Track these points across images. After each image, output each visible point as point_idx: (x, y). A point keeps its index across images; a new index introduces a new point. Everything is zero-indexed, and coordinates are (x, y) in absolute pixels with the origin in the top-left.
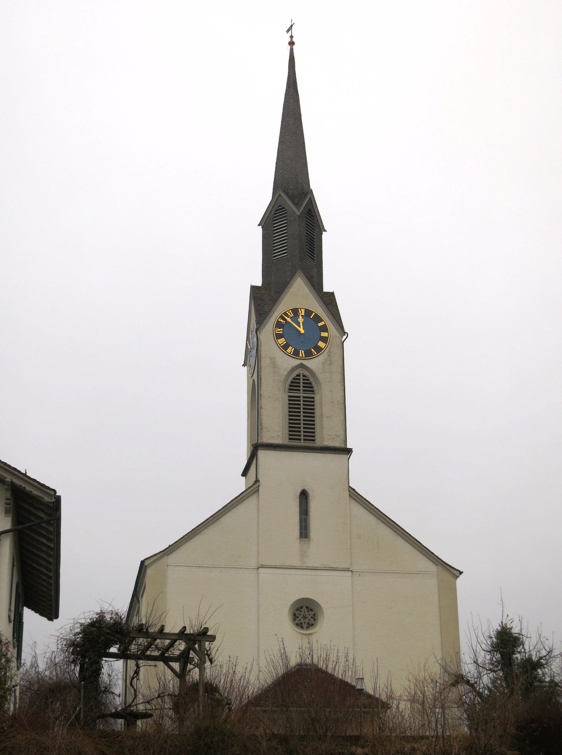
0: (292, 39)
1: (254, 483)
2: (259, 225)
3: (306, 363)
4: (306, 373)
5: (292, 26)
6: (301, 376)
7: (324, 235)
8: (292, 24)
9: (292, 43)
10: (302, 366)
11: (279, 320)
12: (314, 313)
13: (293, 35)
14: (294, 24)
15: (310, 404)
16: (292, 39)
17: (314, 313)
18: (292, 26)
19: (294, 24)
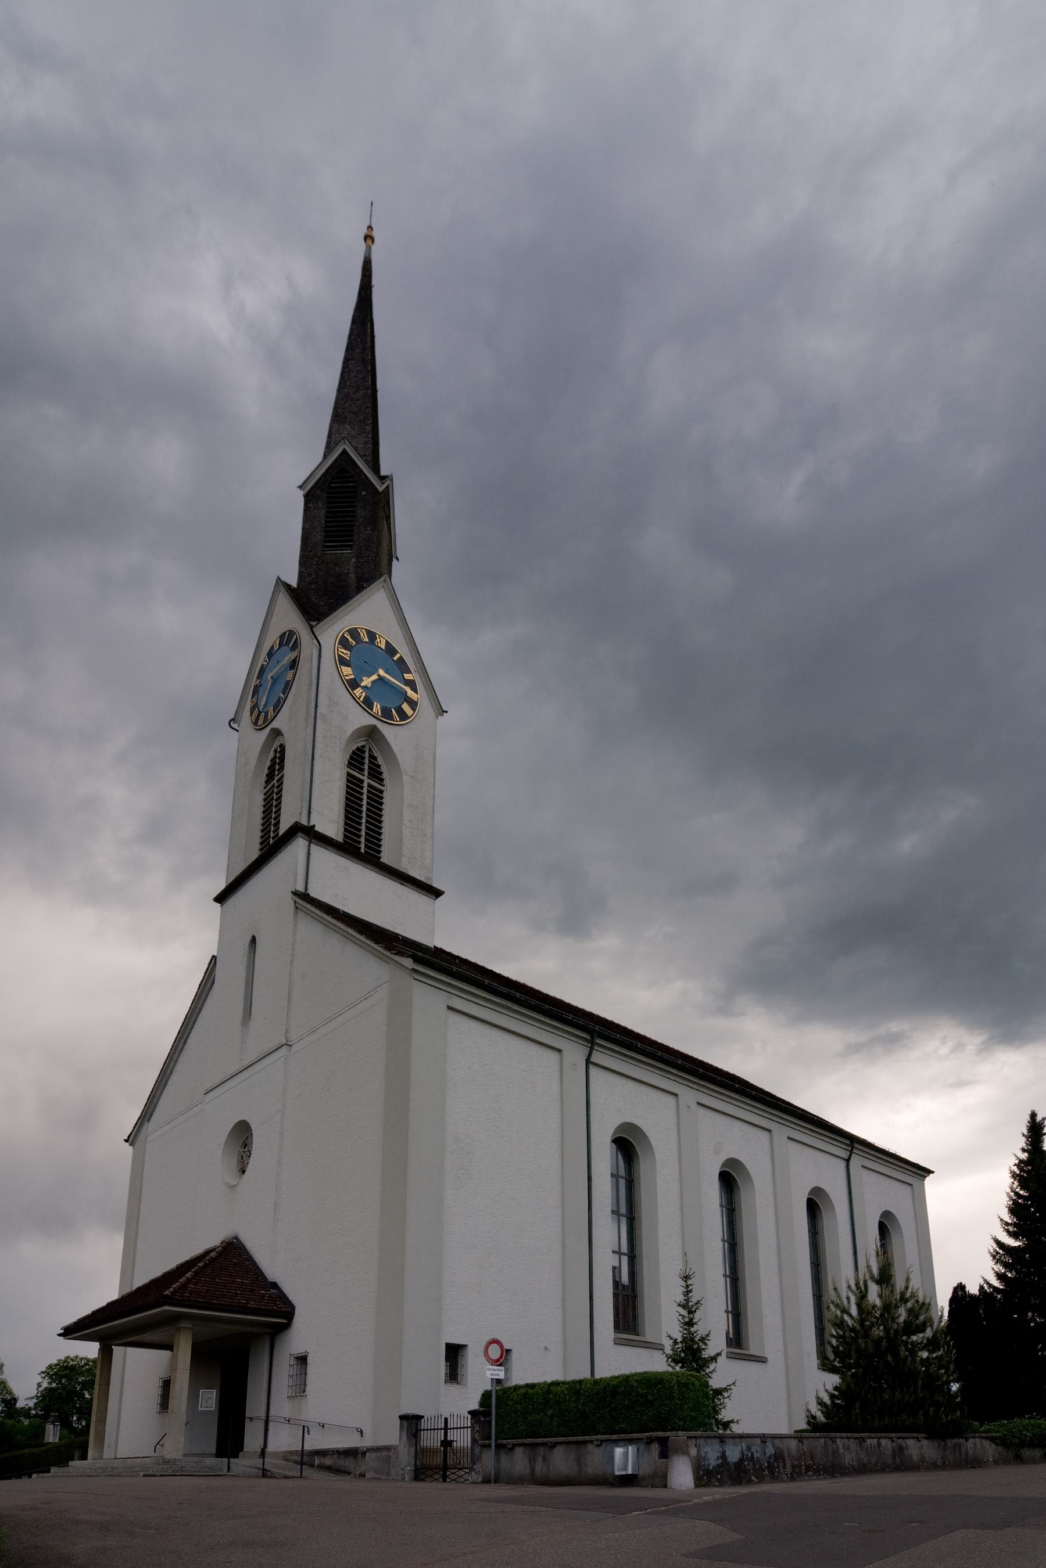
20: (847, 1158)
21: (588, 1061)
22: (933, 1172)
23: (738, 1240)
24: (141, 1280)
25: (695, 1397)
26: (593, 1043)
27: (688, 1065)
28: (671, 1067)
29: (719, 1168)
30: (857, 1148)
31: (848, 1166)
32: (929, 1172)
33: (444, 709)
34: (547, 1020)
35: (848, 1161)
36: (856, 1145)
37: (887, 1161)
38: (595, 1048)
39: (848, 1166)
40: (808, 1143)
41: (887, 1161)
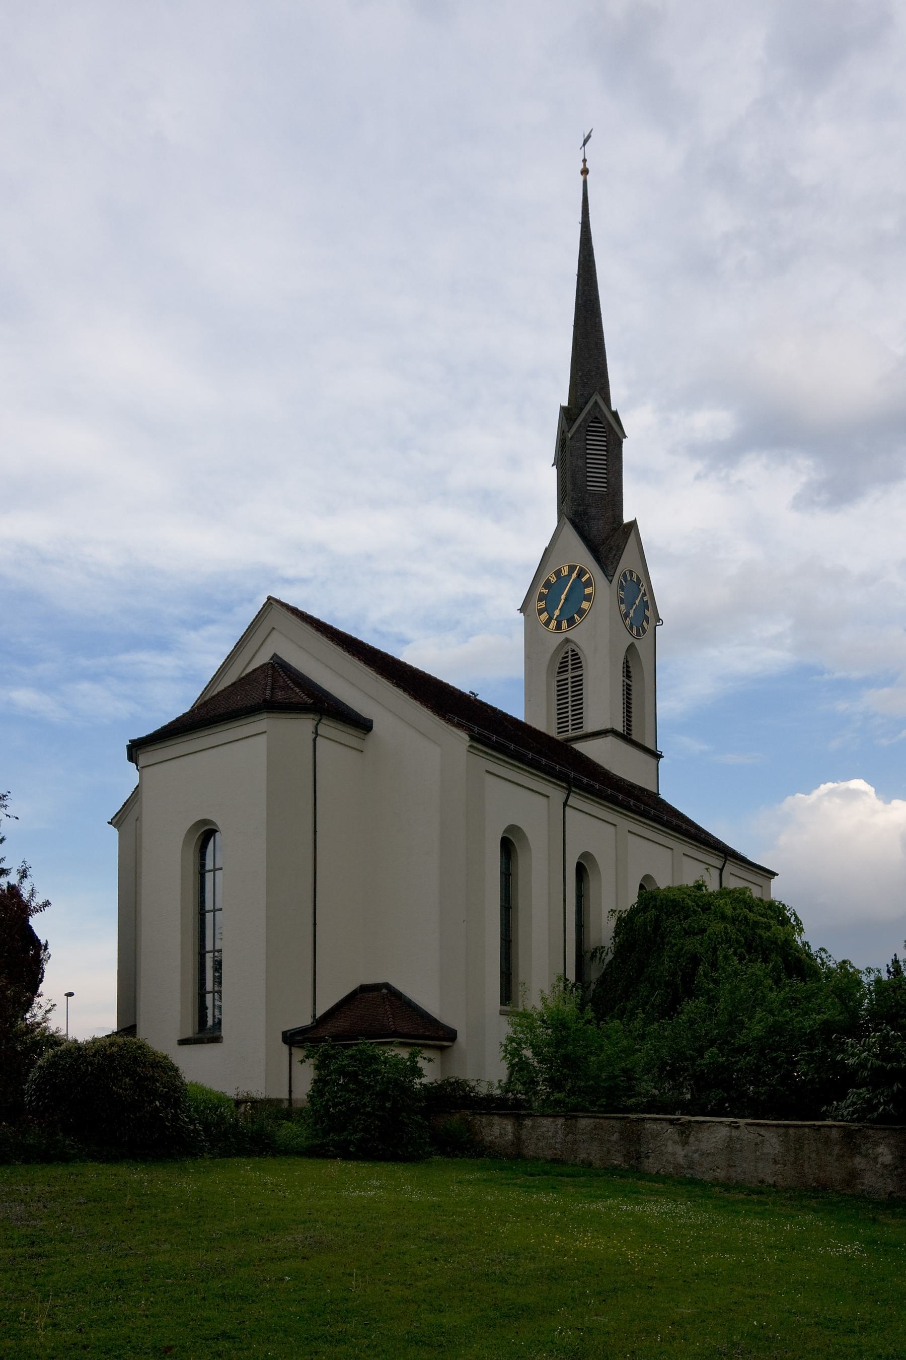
0: (585, 165)
1: (266, 600)
2: (553, 465)
3: (569, 635)
4: (574, 647)
5: (584, 145)
6: (570, 652)
7: (626, 443)
8: (583, 148)
9: (585, 172)
10: (567, 641)
11: (542, 591)
12: (578, 567)
13: (586, 158)
14: (581, 149)
15: (578, 683)
16: (585, 165)
17: (578, 567)
18: (584, 145)
19: (581, 149)
20: (721, 867)
21: (565, 804)
22: (777, 875)
23: (512, 903)
24: (322, 1009)
25: (855, 1116)
26: (726, 860)
27: (675, 821)
28: (517, 761)
29: (502, 833)
30: (729, 860)
31: (721, 875)
32: (774, 874)
33: (660, 618)
34: (490, 751)
35: (721, 870)
36: (729, 858)
37: (504, 761)
38: (727, 862)
39: (721, 875)
40: (534, 789)
41: (504, 761)
